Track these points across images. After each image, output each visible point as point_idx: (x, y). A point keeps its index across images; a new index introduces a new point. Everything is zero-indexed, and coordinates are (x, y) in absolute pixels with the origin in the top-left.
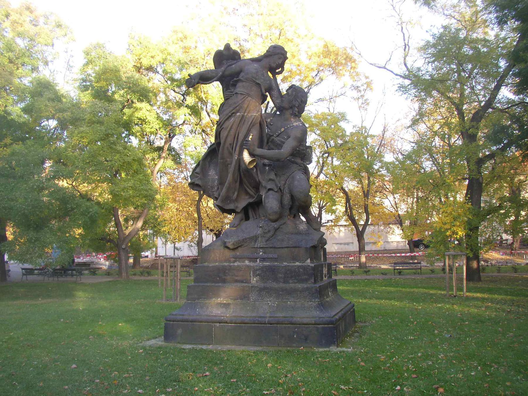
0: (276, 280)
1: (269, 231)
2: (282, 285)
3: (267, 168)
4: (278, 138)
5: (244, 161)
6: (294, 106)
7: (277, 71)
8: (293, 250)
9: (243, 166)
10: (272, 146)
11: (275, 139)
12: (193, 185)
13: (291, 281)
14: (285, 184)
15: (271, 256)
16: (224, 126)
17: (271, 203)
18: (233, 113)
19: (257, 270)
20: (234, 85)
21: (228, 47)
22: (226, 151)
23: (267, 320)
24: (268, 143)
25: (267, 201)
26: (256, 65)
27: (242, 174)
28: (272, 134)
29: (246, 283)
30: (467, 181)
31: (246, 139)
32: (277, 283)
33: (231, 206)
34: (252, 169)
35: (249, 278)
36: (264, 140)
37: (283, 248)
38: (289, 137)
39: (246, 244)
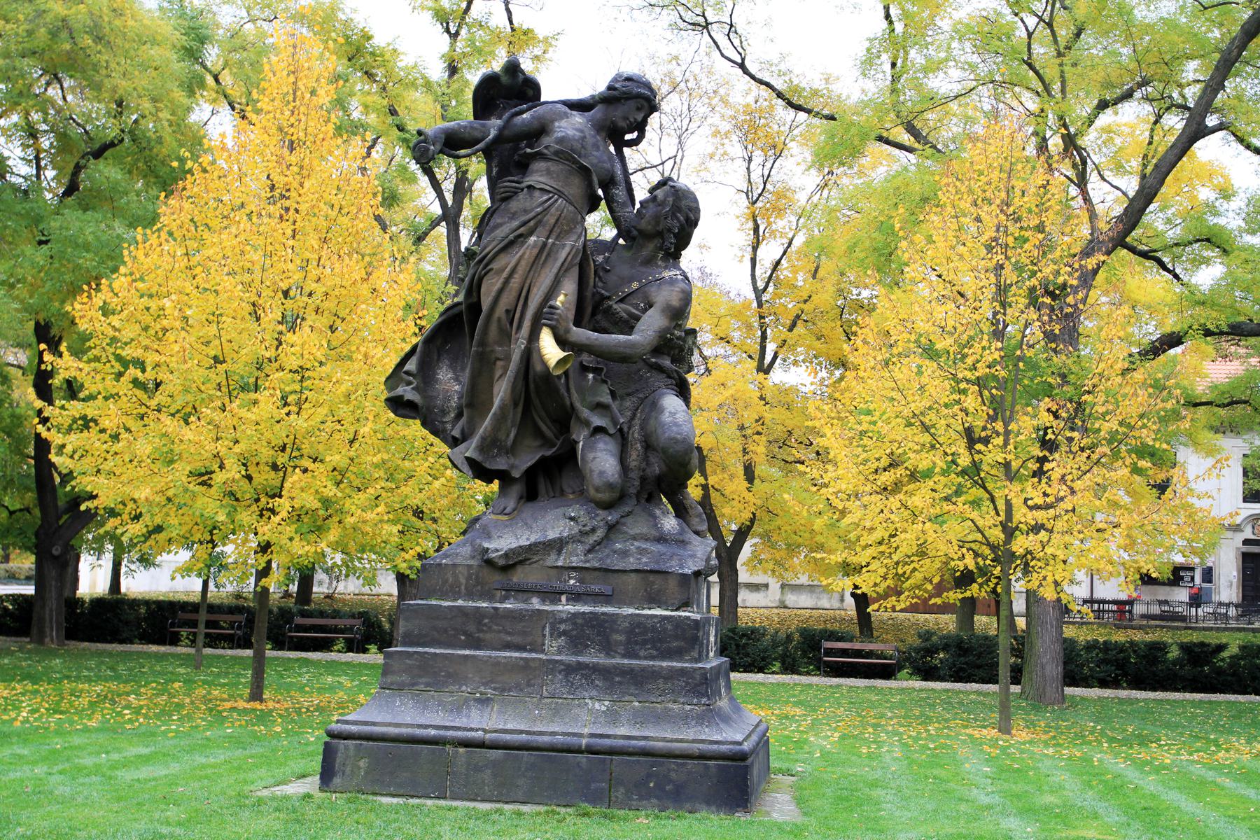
0: (608, 649)
1: (593, 530)
3: (591, 376)
4: (623, 305)
5: (541, 357)
6: (670, 230)
7: (628, 137)
8: (652, 577)
9: (539, 368)
10: (604, 324)
11: (615, 306)
12: (398, 405)
13: (642, 653)
14: (633, 418)
15: (595, 588)
16: (495, 266)
17: (602, 461)
18: (521, 236)
19: (562, 621)
20: (523, 166)
21: (513, 68)
22: (493, 329)
23: (584, 741)
24: (593, 314)
25: (590, 456)
26: (578, 119)
27: (532, 386)
28: (607, 294)
29: (531, 651)
30: (444, 224)
31: (552, 303)
33: (501, 464)
34: (559, 377)
35: (539, 640)
36: (592, 309)
37: (625, 571)
38: (651, 306)
39: (536, 558)
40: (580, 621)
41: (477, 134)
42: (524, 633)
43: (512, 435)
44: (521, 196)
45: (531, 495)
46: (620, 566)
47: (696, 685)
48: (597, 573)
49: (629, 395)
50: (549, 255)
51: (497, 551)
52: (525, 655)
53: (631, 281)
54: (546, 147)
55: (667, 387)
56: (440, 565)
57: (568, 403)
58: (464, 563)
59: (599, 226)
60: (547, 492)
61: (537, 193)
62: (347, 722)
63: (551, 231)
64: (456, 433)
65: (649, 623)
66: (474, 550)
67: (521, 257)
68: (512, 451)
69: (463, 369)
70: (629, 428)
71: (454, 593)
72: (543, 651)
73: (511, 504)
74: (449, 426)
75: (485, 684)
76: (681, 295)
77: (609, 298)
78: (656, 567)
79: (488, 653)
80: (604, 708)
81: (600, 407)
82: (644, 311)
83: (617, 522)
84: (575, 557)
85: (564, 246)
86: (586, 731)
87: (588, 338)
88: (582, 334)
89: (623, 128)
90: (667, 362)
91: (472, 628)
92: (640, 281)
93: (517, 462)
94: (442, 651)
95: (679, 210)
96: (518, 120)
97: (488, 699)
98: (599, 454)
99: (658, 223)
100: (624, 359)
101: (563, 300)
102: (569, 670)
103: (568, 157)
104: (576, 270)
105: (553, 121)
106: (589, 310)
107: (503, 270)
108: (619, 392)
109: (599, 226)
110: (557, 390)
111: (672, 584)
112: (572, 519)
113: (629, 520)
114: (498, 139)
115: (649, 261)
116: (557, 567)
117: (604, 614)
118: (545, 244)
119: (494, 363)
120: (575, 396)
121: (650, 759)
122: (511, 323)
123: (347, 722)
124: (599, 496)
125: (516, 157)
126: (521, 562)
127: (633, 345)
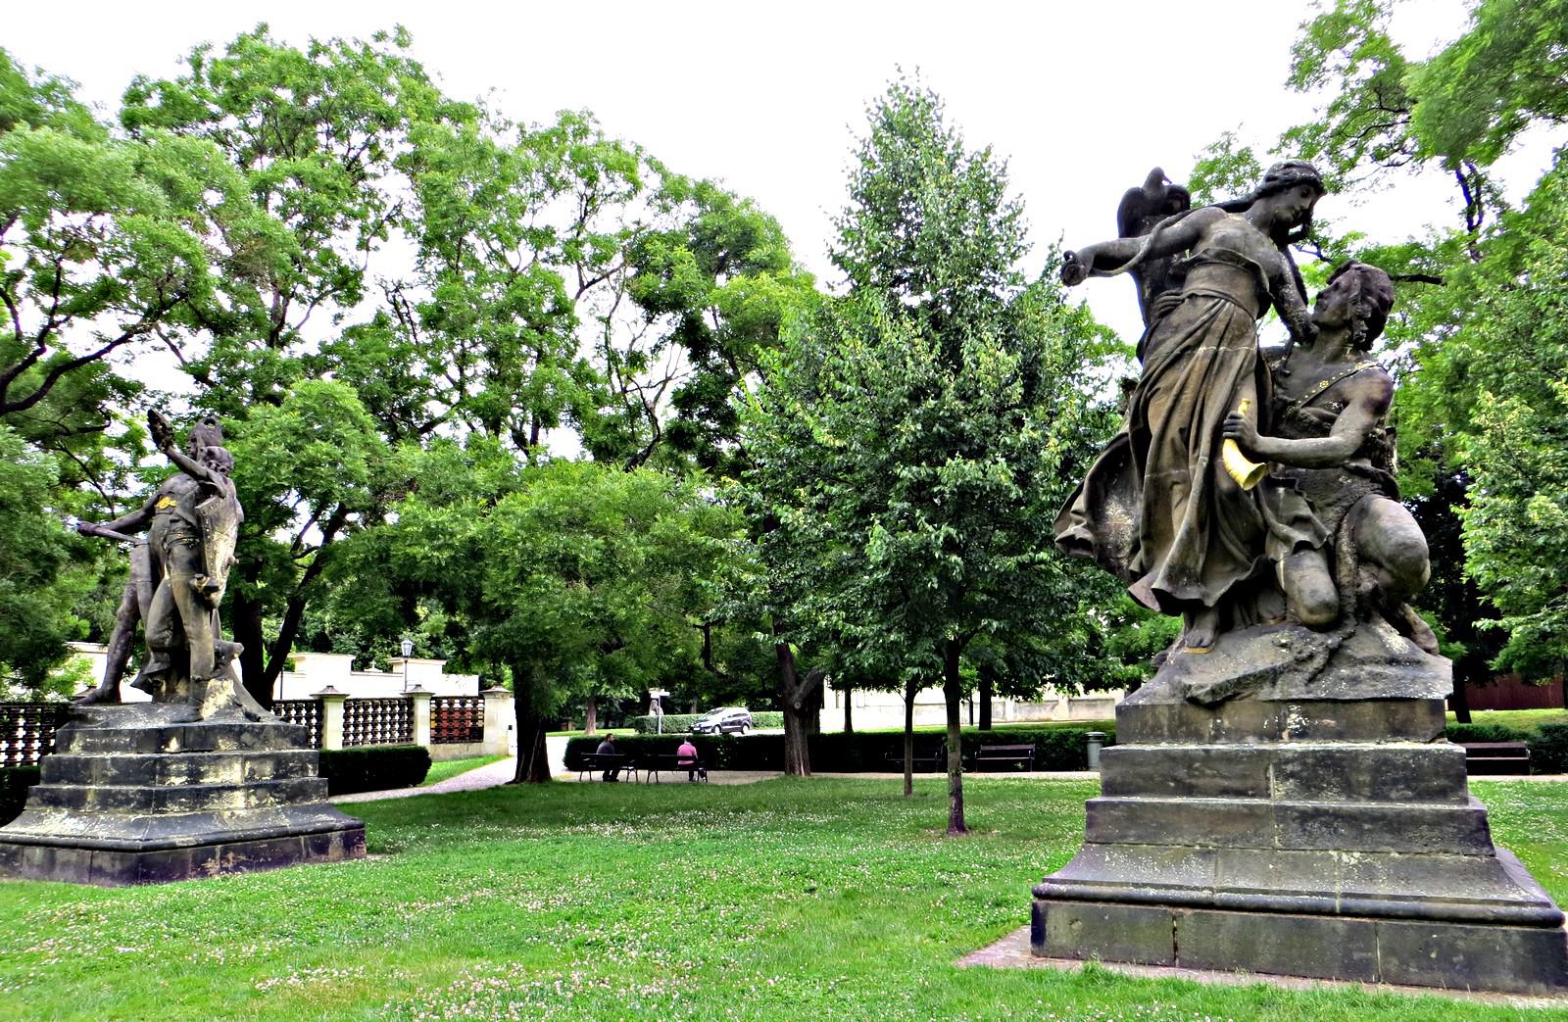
0: (1349, 790)
1: (1311, 657)
2: (1363, 805)
5: (1228, 474)
7: (1292, 231)
8: (1393, 706)
9: (1224, 485)
13: (1393, 795)
17: (1311, 581)
19: (1287, 762)
20: (1180, 279)
25: (1295, 575)
26: (1235, 217)
29: (1253, 796)
32: (1349, 797)
33: (1192, 593)
34: (1248, 493)
35: (1263, 783)
36: (1273, 417)
38: (1345, 403)
40: (1310, 761)
41: (1127, 251)
42: (1244, 777)
43: (1201, 563)
44: (1182, 307)
45: (1224, 627)
46: (1351, 695)
47: (1472, 832)
48: (1322, 705)
49: (1329, 505)
50: (1222, 364)
51: (1202, 687)
52: (1247, 801)
53: (1317, 380)
54: (1205, 252)
55: (1374, 491)
56: (1137, 706)
57: (1261, 520)
58: (1164, 702)
59: (1272, 332)
60: (1244, 620)
61: (1200, 301)
62: (1052, 881)
63: (1222, 339)
64: (1134, 567)
65: (1399, 760)
66: (1174, 687)
67: (1192, 369)
68: (1202, 579)
69: (1133, 503)
70: (1336, 540)
71: (1155, 734)
72: (1268, 796)
73: (1208, 635)
74: (1124, 562)
75: (1205, 835)
76: (1383, 386)
77: (1293, 403)
78: (1398, 694)
79: (1204, 800)
80: (1353, 861)
81: (1298, 521)
82: (1339, 411)
83: (1340, 646)
84: (1294, 687)
85: (1237, 352)
86: (1338, 888)
87: (1280, 446)
88: (1270, 443)
89: (1288, 220)
90: (1367, 464)
91: (1182, 773)
92: (1329, 379)
93: (1208, 591)
94: (1156, 800)
95: (1369, 292)
96: (1167, 231)
97: (1209, 852)
98: (1307, 572)
99: (1344, 312)
100: (1323, 462)
101: (1246, 407)
102: (1305, 816)
103: (1231, 257)
104: (1251, 381)
105: (1208, 224)
106: (1270, 419)
107: (1172, 388)
108: (1319, 503)
109: (1272, 332)
110: (1248, 507)
111: (1421, 712)
112: (1283, 646)
113: (1353, 642)
114: (1150, 255)
115: (1336, 357)
116: (1273, 701)
117: (1339, 751)
118: (1216, 354)
119: (1171, 488)
120: (1269, 512)
121: (1426, 923)
122: (1187, 444)
123: (1052, 881)
124: (1315, 618)
125: (1171, 271)
126: (1230, 698)
127: (1334, 447)
